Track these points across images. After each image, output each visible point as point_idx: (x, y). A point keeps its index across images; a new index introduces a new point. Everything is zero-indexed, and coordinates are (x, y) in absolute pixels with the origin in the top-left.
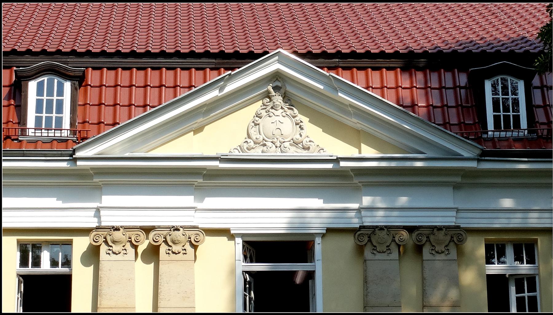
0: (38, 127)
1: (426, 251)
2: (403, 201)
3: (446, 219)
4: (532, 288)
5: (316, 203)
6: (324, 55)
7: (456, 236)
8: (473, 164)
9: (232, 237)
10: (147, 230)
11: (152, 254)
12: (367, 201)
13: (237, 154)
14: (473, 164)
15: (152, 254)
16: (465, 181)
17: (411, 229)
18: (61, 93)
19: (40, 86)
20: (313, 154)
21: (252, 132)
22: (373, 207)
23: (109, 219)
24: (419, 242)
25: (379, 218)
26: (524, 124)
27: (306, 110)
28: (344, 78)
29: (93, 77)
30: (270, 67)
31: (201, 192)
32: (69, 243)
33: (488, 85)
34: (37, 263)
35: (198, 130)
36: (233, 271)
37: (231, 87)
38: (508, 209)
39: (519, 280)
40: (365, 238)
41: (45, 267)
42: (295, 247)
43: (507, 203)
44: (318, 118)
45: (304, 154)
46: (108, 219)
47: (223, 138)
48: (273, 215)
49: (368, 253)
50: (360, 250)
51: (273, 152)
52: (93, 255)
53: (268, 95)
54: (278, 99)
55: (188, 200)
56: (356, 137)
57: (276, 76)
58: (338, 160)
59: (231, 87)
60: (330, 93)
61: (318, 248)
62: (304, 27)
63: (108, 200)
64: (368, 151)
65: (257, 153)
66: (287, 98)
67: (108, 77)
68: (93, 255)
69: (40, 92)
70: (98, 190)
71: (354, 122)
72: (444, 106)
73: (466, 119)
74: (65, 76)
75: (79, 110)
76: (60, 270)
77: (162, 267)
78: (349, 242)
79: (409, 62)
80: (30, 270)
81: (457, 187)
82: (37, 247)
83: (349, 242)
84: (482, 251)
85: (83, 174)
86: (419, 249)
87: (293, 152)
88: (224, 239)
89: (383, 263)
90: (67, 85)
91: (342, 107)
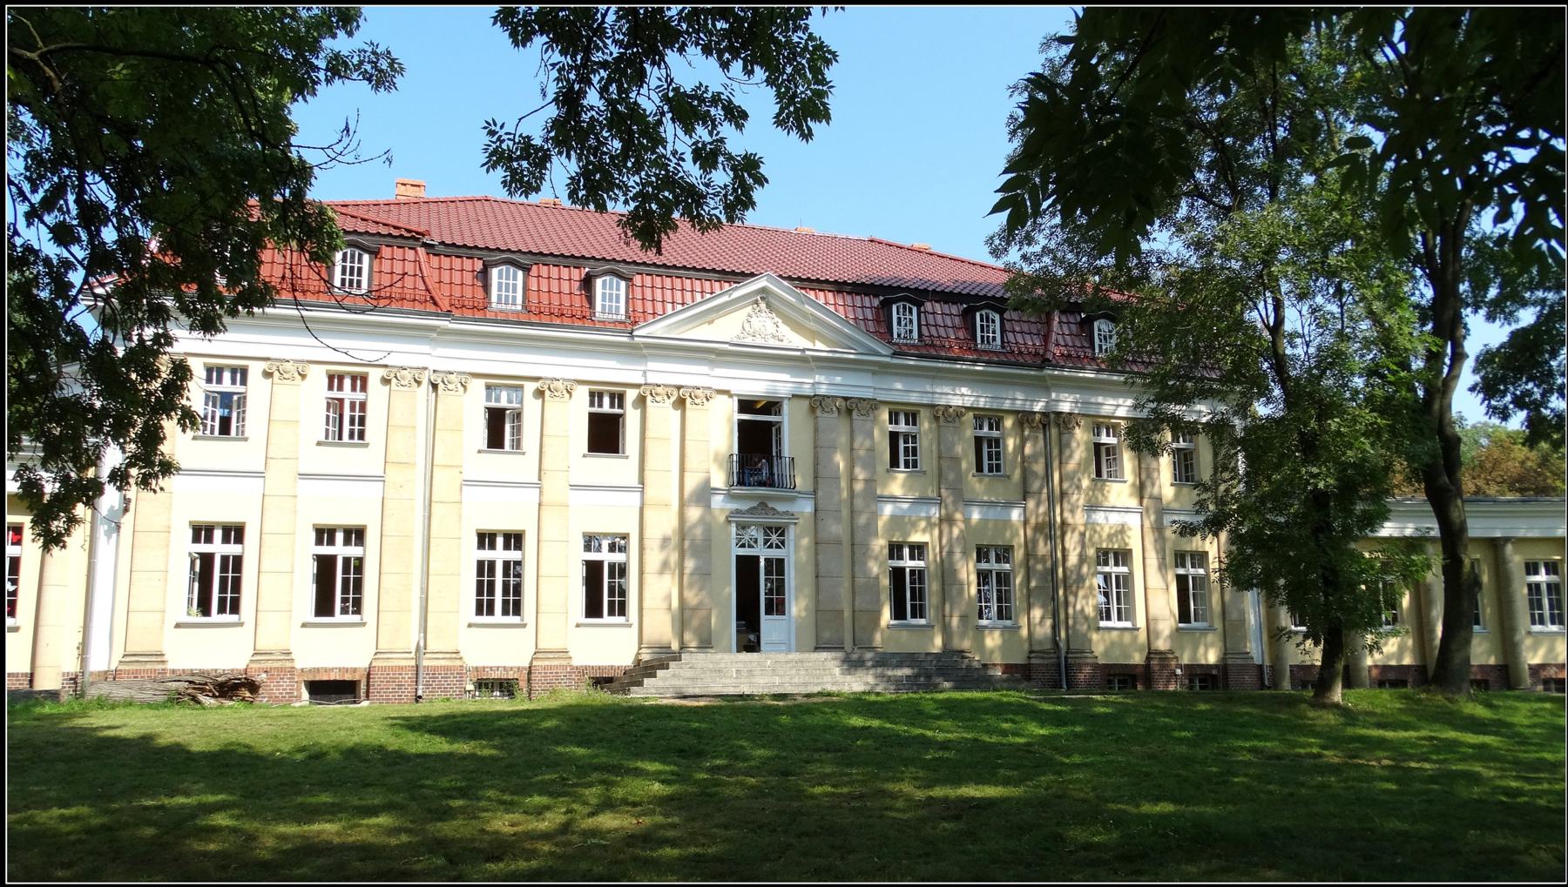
0: (499, 302)
1: (855, 413)
2: (838, 379)
3: (869, 394)
4: (997, 446)
5: (785, 377)
6: (799, 279)
7: (874, 405)
8: (888, 359)
9: (731, 396)
10: (679, 388)
11: (540, 394)
12: (818, 378)
13: (736, 341)
14: (888, 359)
15: (681, 403)
16: (881, 370)
17: (846, 399)
18: (515, 278)
19: (500, 272)
20: (784, 344)
21: (747, 326)
22: (823, 383)
23: (652, 378)
24: (851, 407)
25: (823, 390)
26: (365, 285)
27: (780, 314)
28: (812, 295)
29: (637, 280)
30: (761, 283)
31: (713, 364)
32: (521, 387)
33: (894, 308)
34: (600, 405)
35: (711, 322)
36: (730, 420)
37: (736, 294)
38: (900, 390)
39: (906, 436)
40: (817, 403)
41: (606, 408)
42: (772, 406)
43: (899, 386)
44: (788, 321)
45: (778, 344)
46: (652, 378)
47: (726, 329)
48: (758, 383)
49: (819, 412)
50: (812, 410)
51: (759, 342)
52: (641, 401)
53: (756, 302)
54: (763, 305)
55: (704, 369)
56: (812, 335)
57: (763, 290)
58: (803, 350)
59: (736, 294)
60: (799, 305)
61: (786, 408)
62: (522, 228)
63: (652, 365)
64: (819, 345)
65: (749, 341)
66: (768, 306)
67: (398, 253)
68: (641, 401)
69: (500, 277)
70: (644, 357)
71: (812, 325)
72: (865, 319)
73: (882, 325)
74: (621, 276)
75: (376, 276)
76: (616, 411)
77: (688, 413)
78: (806, 403)
79: (839, 287)
80: (596, 409)
81: (874, 373)
82: (220, 370)
83: (806, 403)
84: (886, 416)
85: (636, 347)
86: (849, 412)
87: (772, 343)
88: (725, 397)
89: (828, 419)
90: (623, 284)
91: (805, 315)
